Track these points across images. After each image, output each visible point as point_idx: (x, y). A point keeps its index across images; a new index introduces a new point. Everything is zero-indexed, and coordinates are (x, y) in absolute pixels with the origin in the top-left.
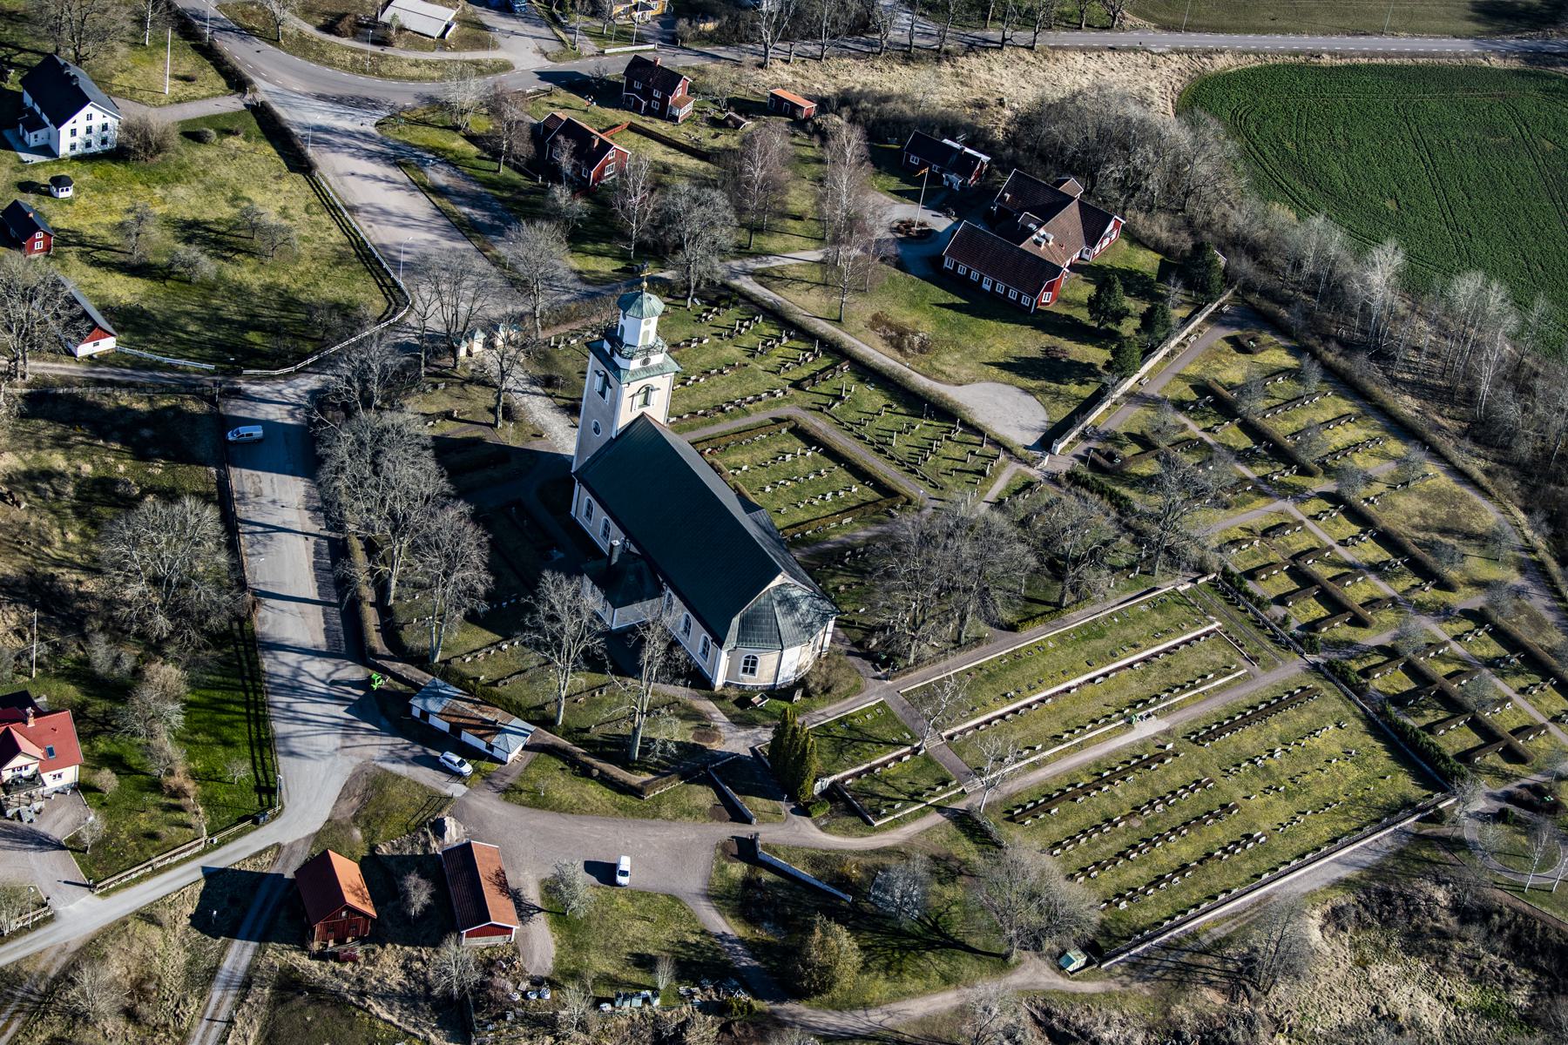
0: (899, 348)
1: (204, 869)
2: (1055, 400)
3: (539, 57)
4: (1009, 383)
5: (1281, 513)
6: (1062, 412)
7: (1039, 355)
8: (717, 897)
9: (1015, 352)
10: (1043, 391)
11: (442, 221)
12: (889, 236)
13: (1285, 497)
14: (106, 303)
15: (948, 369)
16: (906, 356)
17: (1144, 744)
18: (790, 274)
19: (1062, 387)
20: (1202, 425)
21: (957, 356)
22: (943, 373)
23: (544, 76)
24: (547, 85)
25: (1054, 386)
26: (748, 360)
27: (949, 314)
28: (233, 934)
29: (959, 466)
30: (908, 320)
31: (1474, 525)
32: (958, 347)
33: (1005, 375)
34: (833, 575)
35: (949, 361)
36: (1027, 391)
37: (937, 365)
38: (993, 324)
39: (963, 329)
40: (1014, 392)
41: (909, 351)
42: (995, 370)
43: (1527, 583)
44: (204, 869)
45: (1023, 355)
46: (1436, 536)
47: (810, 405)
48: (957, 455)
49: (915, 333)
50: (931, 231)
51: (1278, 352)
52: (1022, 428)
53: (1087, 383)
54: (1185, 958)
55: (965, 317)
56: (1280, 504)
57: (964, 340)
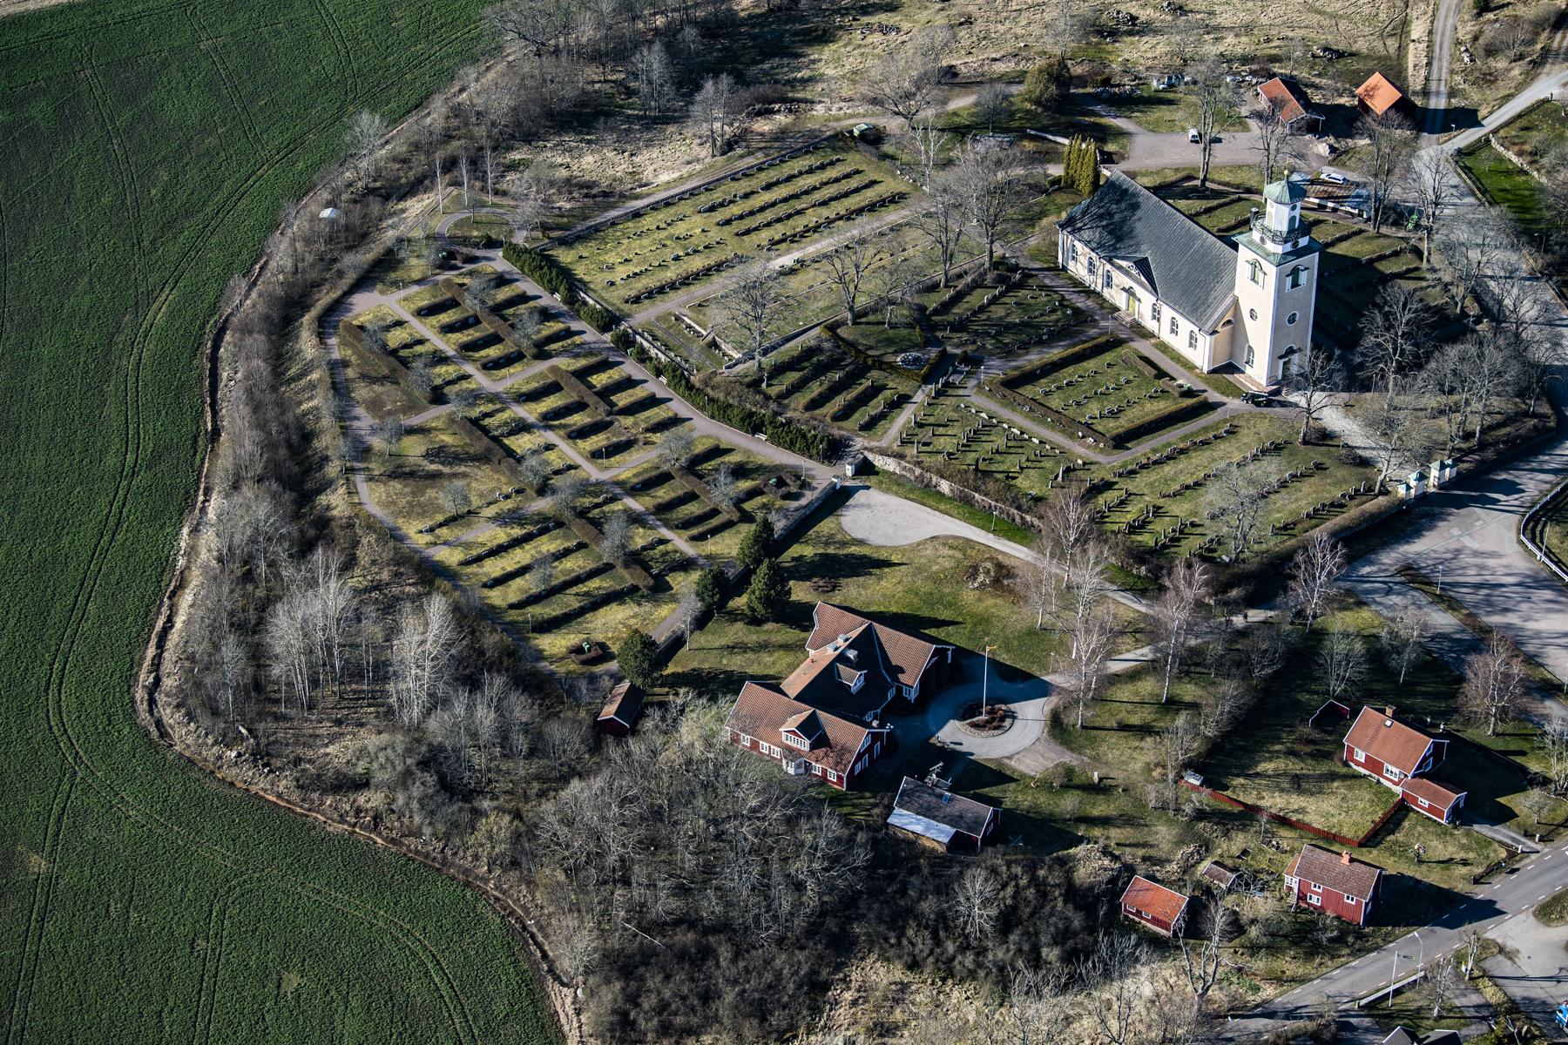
0: (1000, 566)
1: (1481, 125)
2: (832, 536)
3: (1510, 944)
4: (878, 548)
5: (607, 468)
6: (826, 526)
7: (843, 581)
8: (1120, 134)
9: (871, 580)
10: (844, 544)
11: (1530, 648)
12: (1014, 707)
13: (598, 483)
14: (1553, 20)
15: (946, 551)
16: (991, 559)
17: (788, 251)
18: (1128, 639)
19: (821, 551)
20: (669, 547)
21: (935, 568)
22: (951, 547)
23: (1488, 910)
24: (1481, 892)
25: (831, 551)
26: (1160, 502)
27: (945, 615)
28: (1446, 111)
29: (941, 430)
30: (990, 602)
31: (399, 486)
32: (936, 579)
33: (883, 555)
34: (1058, 321)
35: (945, 560)
36: (861, 542)
37: (959, 555)
38: (894, 609)
39: (930, 600)
40: (875, 540)
41: (989, 565)
42: (895, 559)
43: (367, 438)
44: (1481, 125)
45: (861, 579)
46: (446, 470)
47: (1093, 467)
48: (942, 440)
49: (982, 584)
50: (963, 718)
51: (555, 650)
52: (869, 506)
53: (794, 559)
54: (777, 144)
55: (925, 612)
56: (605, 476)
57: (927, 587)
